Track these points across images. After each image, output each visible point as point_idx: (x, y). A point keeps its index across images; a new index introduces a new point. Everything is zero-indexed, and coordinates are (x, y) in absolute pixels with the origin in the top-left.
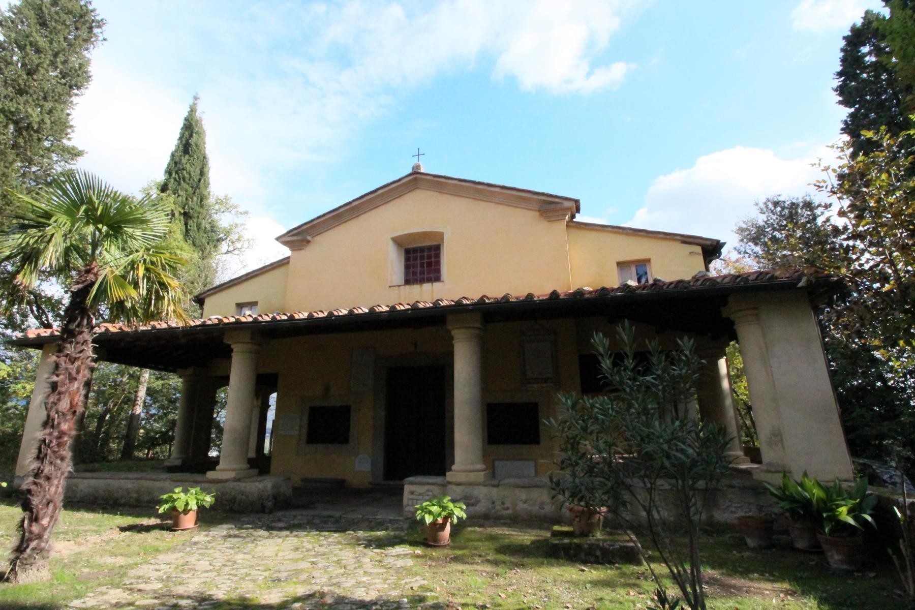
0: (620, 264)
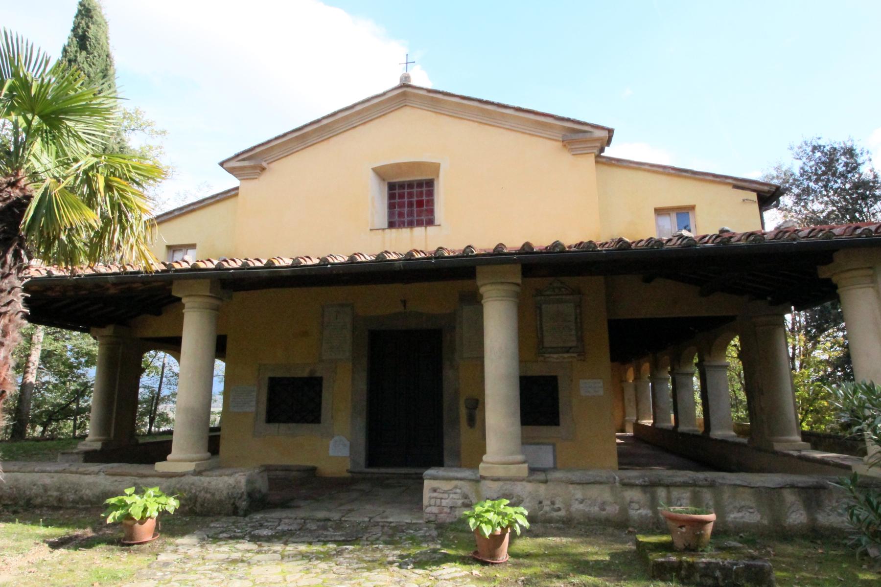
0: (659, 212)
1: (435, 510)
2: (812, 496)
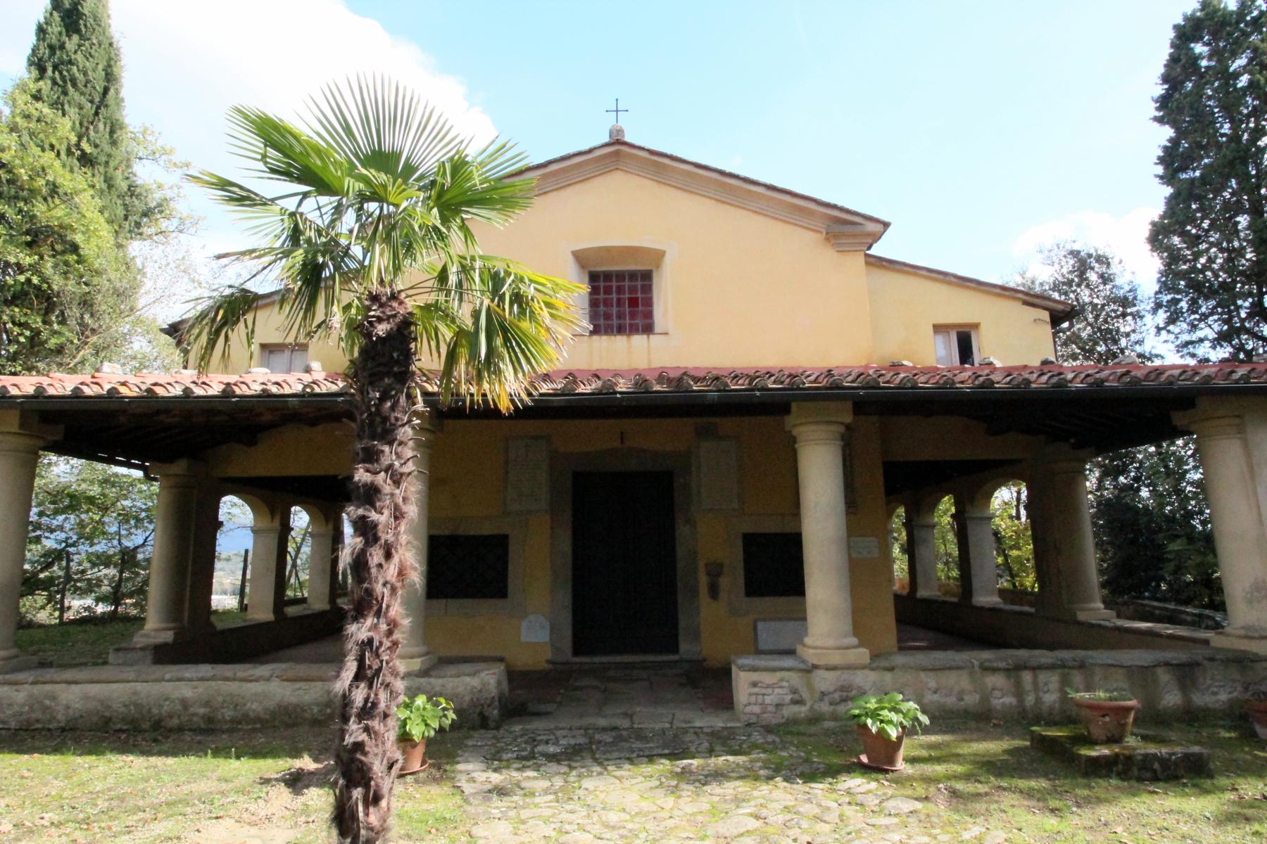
1: (757, 709)
2: (1186, 673)
